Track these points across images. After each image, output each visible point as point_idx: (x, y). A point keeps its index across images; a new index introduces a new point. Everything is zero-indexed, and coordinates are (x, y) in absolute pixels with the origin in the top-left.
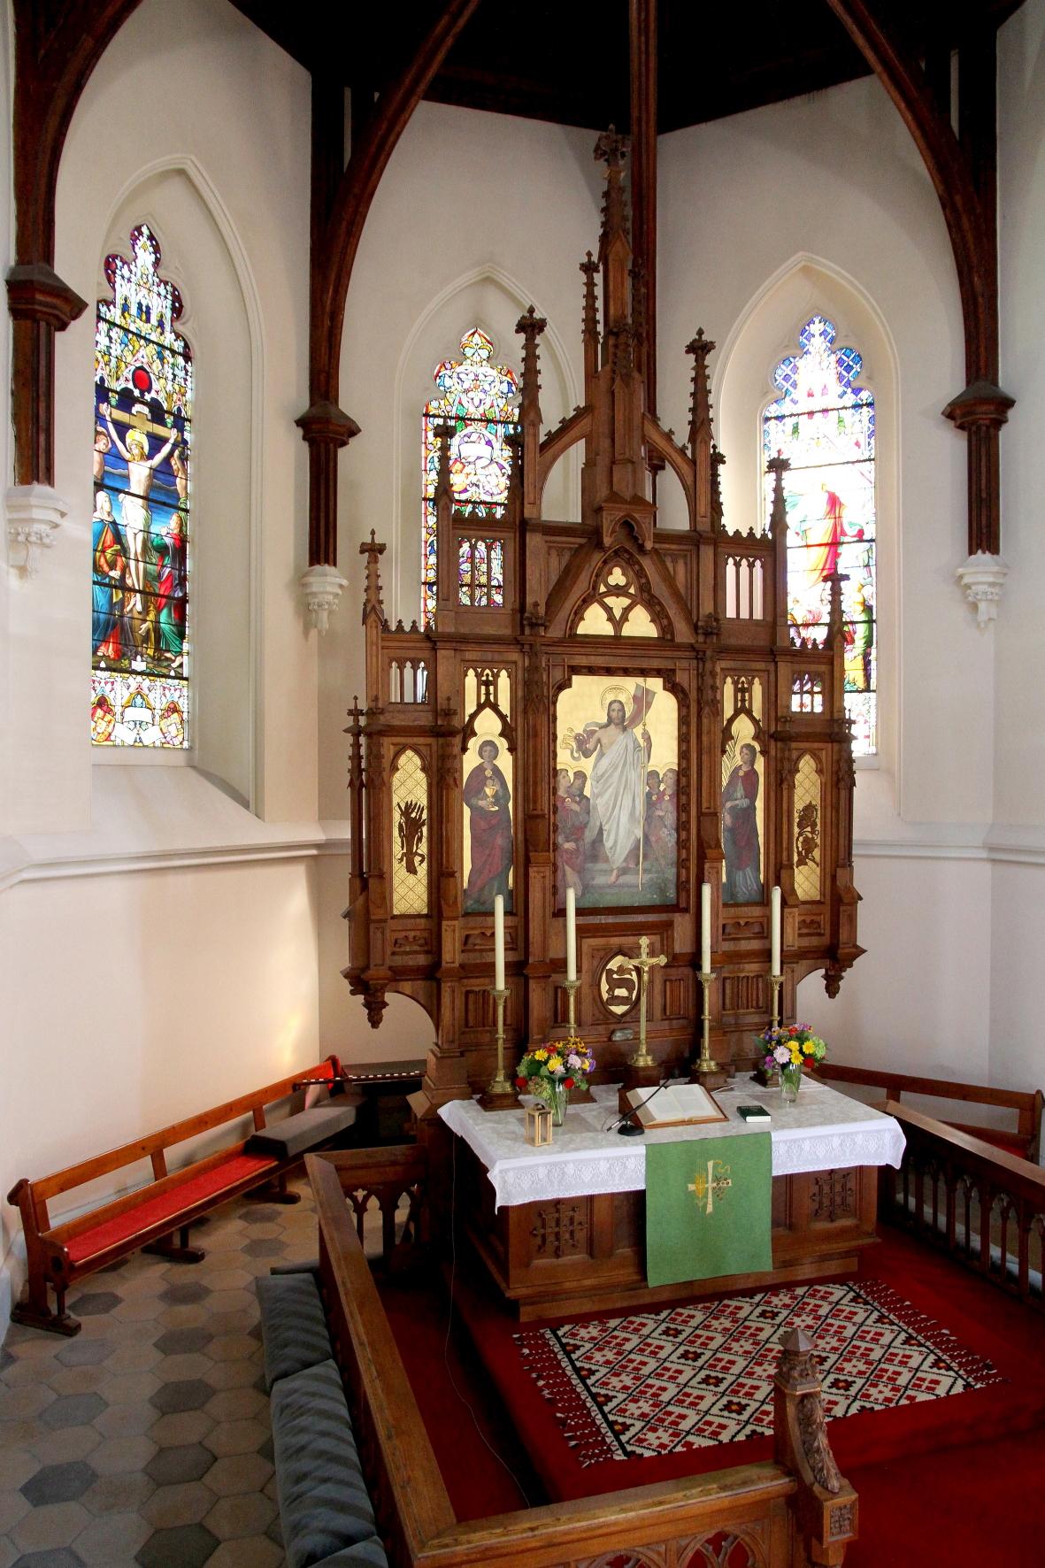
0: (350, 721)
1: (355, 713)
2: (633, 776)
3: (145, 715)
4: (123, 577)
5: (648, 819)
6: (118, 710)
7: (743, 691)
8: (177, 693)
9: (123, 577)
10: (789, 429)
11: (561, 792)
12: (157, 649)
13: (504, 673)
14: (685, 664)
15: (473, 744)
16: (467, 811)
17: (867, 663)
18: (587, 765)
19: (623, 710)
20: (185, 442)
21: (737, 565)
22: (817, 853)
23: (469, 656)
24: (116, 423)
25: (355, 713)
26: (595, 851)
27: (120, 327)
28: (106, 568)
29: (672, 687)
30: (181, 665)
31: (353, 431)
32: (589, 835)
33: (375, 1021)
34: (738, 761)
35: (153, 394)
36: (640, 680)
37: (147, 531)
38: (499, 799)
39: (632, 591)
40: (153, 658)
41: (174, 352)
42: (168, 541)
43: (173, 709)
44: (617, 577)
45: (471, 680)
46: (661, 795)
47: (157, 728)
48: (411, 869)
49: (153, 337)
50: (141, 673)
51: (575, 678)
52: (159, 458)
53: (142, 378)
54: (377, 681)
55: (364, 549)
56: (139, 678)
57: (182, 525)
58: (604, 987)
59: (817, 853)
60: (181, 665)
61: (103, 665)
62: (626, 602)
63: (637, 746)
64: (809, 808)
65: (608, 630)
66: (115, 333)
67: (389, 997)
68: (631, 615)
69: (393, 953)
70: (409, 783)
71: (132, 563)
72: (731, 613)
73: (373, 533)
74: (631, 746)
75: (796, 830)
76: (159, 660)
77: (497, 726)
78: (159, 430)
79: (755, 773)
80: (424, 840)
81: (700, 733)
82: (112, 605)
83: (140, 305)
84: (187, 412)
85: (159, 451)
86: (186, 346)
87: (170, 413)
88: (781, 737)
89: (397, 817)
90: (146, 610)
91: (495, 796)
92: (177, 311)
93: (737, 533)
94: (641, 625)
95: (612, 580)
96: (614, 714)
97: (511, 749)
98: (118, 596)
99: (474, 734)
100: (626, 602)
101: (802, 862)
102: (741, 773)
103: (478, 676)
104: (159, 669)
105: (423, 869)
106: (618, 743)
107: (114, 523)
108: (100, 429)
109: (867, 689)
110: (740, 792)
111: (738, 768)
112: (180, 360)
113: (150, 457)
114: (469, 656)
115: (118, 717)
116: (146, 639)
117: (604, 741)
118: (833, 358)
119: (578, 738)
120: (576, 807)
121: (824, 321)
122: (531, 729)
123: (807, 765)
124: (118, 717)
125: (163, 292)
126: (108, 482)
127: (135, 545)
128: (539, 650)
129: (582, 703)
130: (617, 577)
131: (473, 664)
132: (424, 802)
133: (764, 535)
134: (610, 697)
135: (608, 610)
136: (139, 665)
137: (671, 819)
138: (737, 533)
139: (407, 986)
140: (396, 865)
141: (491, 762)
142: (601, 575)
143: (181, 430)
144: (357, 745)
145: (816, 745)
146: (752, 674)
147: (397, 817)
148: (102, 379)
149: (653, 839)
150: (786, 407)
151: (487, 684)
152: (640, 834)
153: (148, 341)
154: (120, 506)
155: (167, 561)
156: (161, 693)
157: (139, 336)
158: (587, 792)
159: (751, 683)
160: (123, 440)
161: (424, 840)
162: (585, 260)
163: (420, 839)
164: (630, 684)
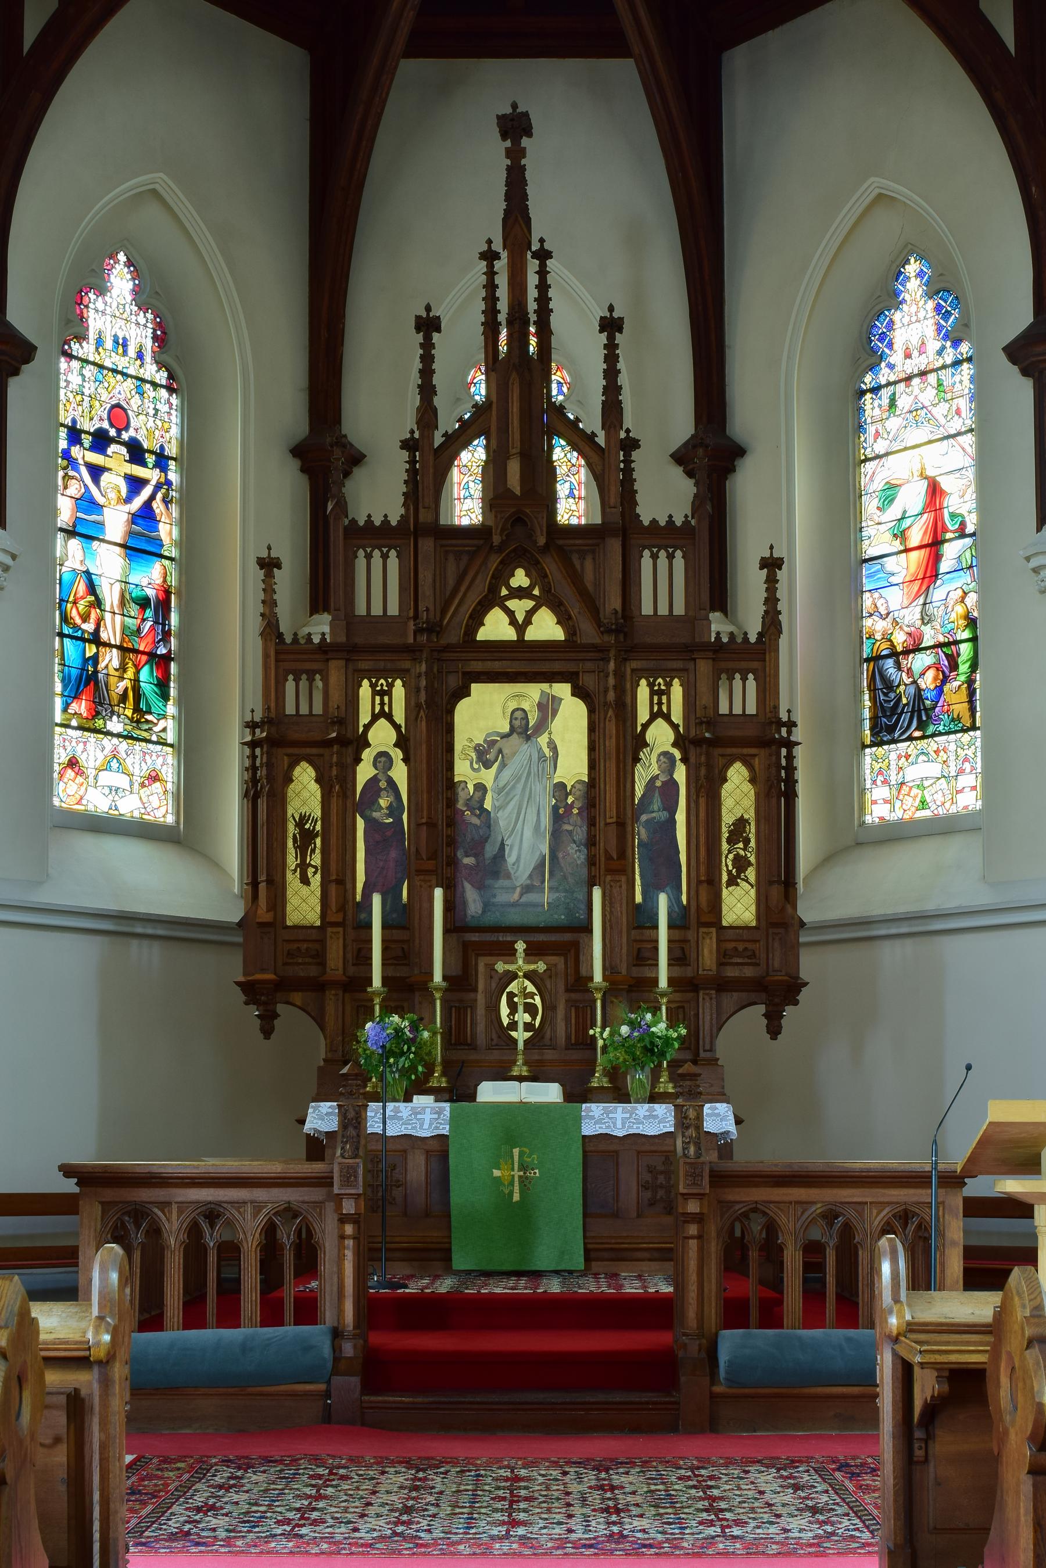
1: (252, 725)
2: (538, 788)
3: (123, 781)
5: (556, 835)
6: (91, 773)
7: (660, 693)
8: (160, 760)
10: (885, 401)
11: (460, 805)
12: (137, 709)
13: (398, 683)
14: (589, 665)
15: (368, 755)
16: (360, 824)
17: (971, 693)
18: (488, 777)
19: (526, 718)
20: (168, 483)
21: (655, 557)
22: (751, 873)
23: (363, 665)
25: (252, 725)
26: (495, 867)
27: (94, 364)
28: (78, 621)
29: (577, 692)
30: (164, 730)
31: (365, 456)
32: (490, 850)
33: (267, 1032)
34: (655, 770)
35: (132, 433)
36: (545, 686)
38: (395, 810)
39: (536, 592)
40: (131, 720)
41: (155, 385)
42: (151, 593)
43: (155, 777)
44: (520, 579)
45: (365, 690)
46: (569, 808)
47: (135, 797)
48: (305, 881)
49: (131, 371)
50: (118, 735)
51: (475, 687)
53: (118, 413)
56: (115, 741)
58: (504, 1011)
59: (751, 873)
61: (74, 723)
62: (529, 604)
63: (542, 757)
64: (741, 823)
65: (511, 634)
66: (89, 371)
67: (280, 1008)
68: (535, 618)
69: (285, 964)
70: (305, 792)
71: (108, 616)
72: (647, 609)
74: (535, 757)
75: (725, 846)
76: (138, 722)
77: (393, 736)
79: (675, 784)
80: (318, 851)
81: (615, 741)
82: (86, 660)
83: (115, 336)
84: (172, 450)
87: (151, 452)
88: (708, 745)
90: (123, 668)
91: (390, 807)
93: (654, 522)
94: (546, 627)
95: (515, 582)
96: (517, 723)
97: (406, 760)
98: (91, 650)
99: (369, 745)
100: (529, 604)
101: (732, 882)
102: (658, 784)
105: (316, 880)
106: (521, 753)
107: (88, 573)
108: (71, 473)
109: (974, 728)
110: (657, 803)
111: (655, 778)
112: (164, 393)
113: (128, 500)
114: (363, 665)
115: (91, 779)
116: (124, 698)
117: (505, 751)
118: (931, 305)
119: (477, 749)
120: (475, 821)
121: (921, 258)
122: (430, 740)
123: (737, 776)
124: (91, 779)
125: (142, 321)
126: (80, 529)
127: (110, 596)
128: (444, 663)
129: (484, 711)
130: (520, 579)
131: (368, 674)
132: (318, 813)
133: (686, 522)
134: (512, 705)
135: (510, 614)
136: (115, 725)
137: (581, 833)
138: (654, 522)
139: (297, 997)
140: (289, 876)
142: (503, 575)
143: (164, 469)
144: (253, 757)
145: (746, 751)
146: (669, 674)
147: (291, 828)
148: (74, 421)
149: (560, 855)
150: (884, 375)
151: (382, 693)
152: (546, 851)
154: (94, 554)
155: (149, 613)
156: (140, 759)
157: (115, 371)
158: (488, 805)
159: (669, 685)
161: (318, 851)
162: (485, 248)
163: (313, 851)
164: (532, 693)
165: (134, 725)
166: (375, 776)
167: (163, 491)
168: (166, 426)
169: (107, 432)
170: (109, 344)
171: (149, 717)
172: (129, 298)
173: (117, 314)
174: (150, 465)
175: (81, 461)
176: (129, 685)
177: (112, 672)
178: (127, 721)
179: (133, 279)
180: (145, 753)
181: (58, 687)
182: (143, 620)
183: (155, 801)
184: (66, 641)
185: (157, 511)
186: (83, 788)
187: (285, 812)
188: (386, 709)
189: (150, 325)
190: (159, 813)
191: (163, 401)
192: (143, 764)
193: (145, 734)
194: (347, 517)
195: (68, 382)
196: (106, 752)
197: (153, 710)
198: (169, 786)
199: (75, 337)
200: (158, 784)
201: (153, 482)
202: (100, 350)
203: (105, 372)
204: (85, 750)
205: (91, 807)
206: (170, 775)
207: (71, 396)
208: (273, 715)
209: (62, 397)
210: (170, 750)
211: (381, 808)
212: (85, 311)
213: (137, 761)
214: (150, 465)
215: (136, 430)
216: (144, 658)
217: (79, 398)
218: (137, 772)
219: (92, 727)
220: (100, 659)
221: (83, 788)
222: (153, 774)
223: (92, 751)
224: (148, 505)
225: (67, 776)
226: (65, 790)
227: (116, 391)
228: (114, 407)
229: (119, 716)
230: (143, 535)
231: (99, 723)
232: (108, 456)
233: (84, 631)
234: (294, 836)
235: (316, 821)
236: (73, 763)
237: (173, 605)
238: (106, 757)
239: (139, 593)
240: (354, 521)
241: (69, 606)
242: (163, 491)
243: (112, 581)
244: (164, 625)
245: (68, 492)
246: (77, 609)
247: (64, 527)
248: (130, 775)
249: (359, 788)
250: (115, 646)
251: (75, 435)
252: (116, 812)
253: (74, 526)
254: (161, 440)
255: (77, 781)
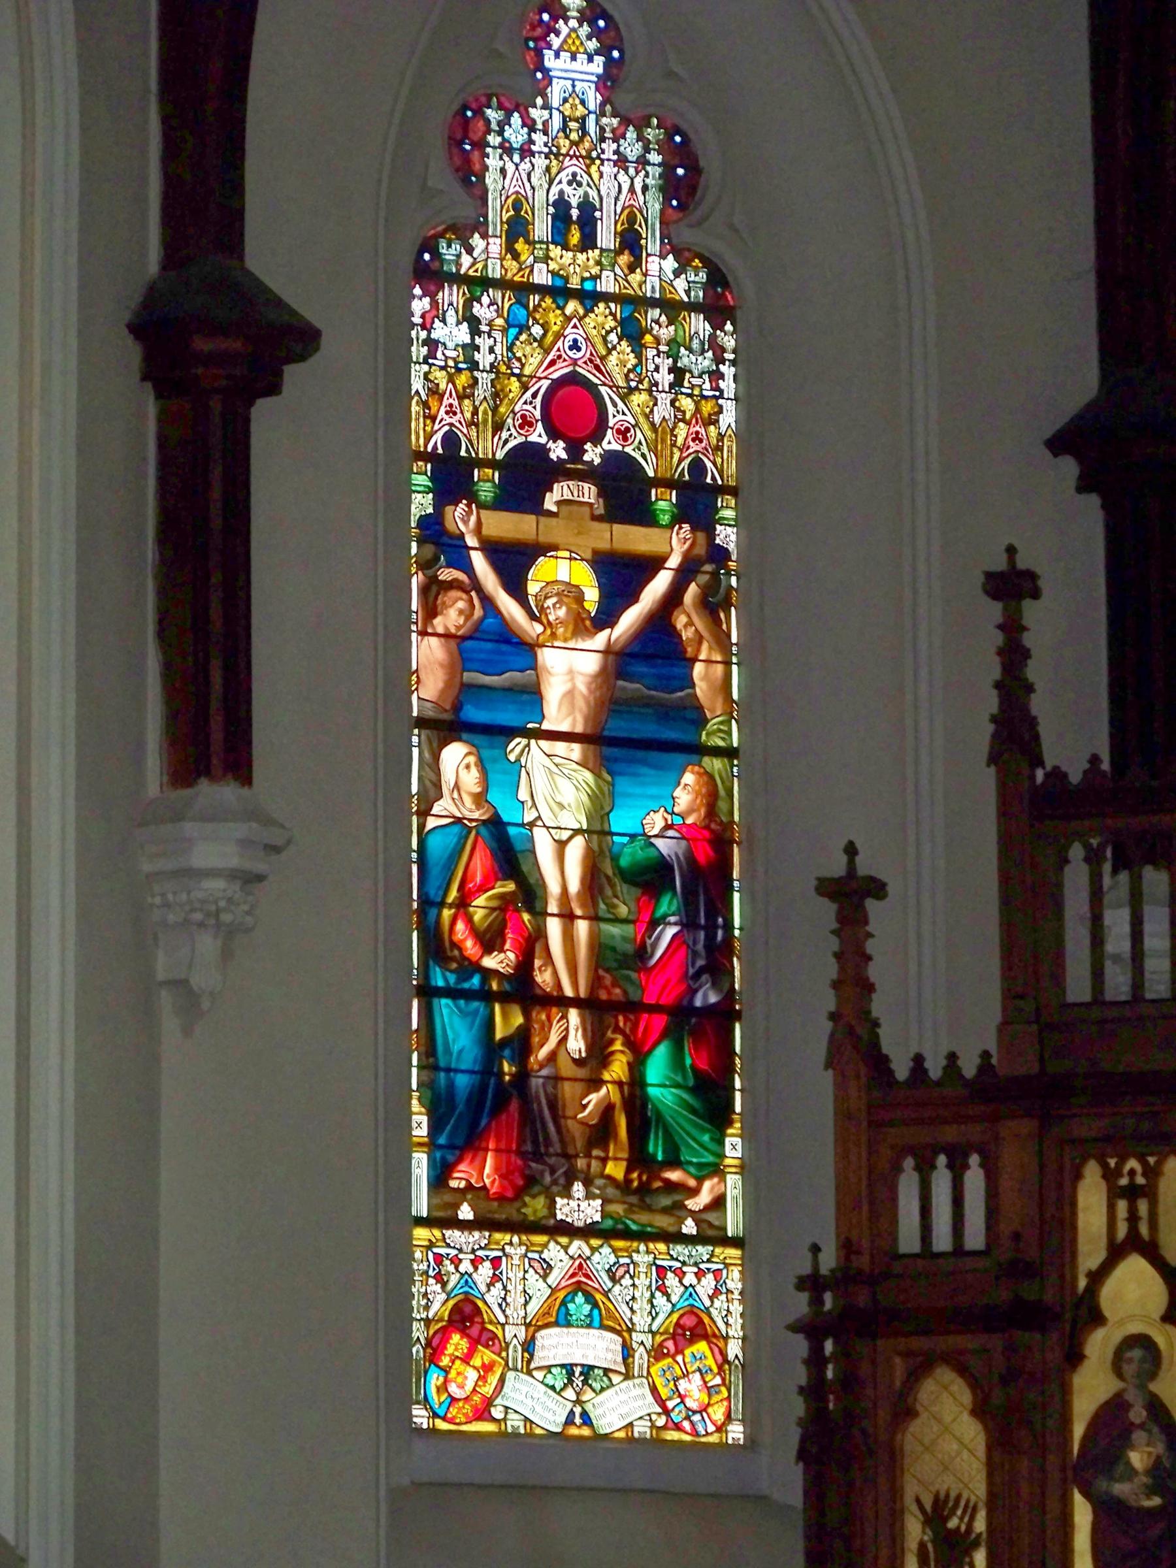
0: (800, 1304)
1: (812, 1284)
3: (598, 1348)
4: (524, 967)
6: (515, 1333)
9: (524, 967)
12: (638, 1158)
15: (1099, 1345)
16: (1083, 1514)
20: (719, 555)
24: (496, 551)
25: (812, 1284)
28: (470, 946)
30: (718, 1203)
35: (611, 443)
37: (597, 831)
41: (672, 308)
49: (607, 284)
50: (588, 1232)
52: (630, 618)
53: (574, 407)
54: (866, 1201)
55: (829, 888)
56: (578, 1246)
57: (712, 797)
60: (718, 1203)
61: (466, 1212)
70: (947, 1442)
71: (554, 927)
73: (851, 850)
78: (634, 539)
82: (491, 1049)
83: (561, 204)
84: (724, 467)
85: (634, 599)
86: (717, 279)
87: (669, 484)
89: (914, 1530)
90: (598, 1055)
92: (682, 189)
98: (507, 1021)
103: (1110, 1176)
104: (647, 1208)
107: (496, 824)
112: (699, 325)
113: (606, 618)
115: (515, 1353)
116: (602, 1131)
126: (474, 713)
127: (561, 870)
132: (978, 1489)
136: (578, 1207)
141: (1142, 1387)
144: (816, 1361)
147: (914, 1530)
151: (1132, 1193)
153: (590, 299)
156: (645, 1288)
157: (560, 292)
160: (516, 589)
165: (634, 1199)
166: (1118, 1395)
167: (703, 579)
168: (707, 408)
169: (543, 450)
170: (542, 227)
171: (674, 1176)
172: (593, 99)
173: (565, 149)
174: (665, 519)
175: (471, 541)
176: (616, 1097)
177: (566, 1068)
178: (611, 1191)
179: (604, 51)
180: (661, 1271)
181: (420, 1126)
182: (654, 923)
183: (693, 1388)
184: (444, 1007)
185: (687, 635)
186: (493, 1379)
187: (896, 1493)
188: (1144, 1230)
189: (655, 158)
190: (707, 1428)
191: (695, 345)
192: (660, 1300)
193: (663, 1222)
194: (1041, 764)
195: (432, 345)
196: (553, 1279)
197: (685, 1156)
198: (734, 1349)
199: (452, 228)
200: (702, 1347)
201: (674, 562)
202: (520, 246)
203: (534, 299)
204: (496, 1278)
205: (515, 1423)
206: (736, 1321)
207: (440, 377)
208: (863, 1262)
209: (417, 384)
210: (734, 1252)
211: (1133, 1472)
212: (476, 155)
213: (642, 1294)
214: (665, 519)
215: (623, 434)
216: (662, 1020)
217: (463, 380)
218: (641, 1320)
219: (515, 1217)
220: (536, 1040)
221: (493, 1379)
222: (689, 1321)
223: (518, 1280)
224: (660, 621)
225: (450, 1349)
226: (443, 1388)
227: (564, 344)
228: (557, 384)
229: (587, 1183)
230: (647, 703)
231: (535, 1206)
232: (550, 514)
233: (487, 973)
234: (922, 1546)
235: (975, 1509)
236: (466, 1316)
237: (736, 874)
238: (554, 1290)
239: (641, 855)
240: (1057, 775)
241: (447, 913)
242: (703, 579)
243: (565, 835)
244: (711, 929)
245: (439, 624)
246: (469, 921)
247: (430, 714)
248: (624, 1331)
249: (1078, 1430)
250: (576, 1002)
251: (452, 475)
252: (586, 1432)
253: (457, 707)
254: (694, 447)
255: (477, 1361)
